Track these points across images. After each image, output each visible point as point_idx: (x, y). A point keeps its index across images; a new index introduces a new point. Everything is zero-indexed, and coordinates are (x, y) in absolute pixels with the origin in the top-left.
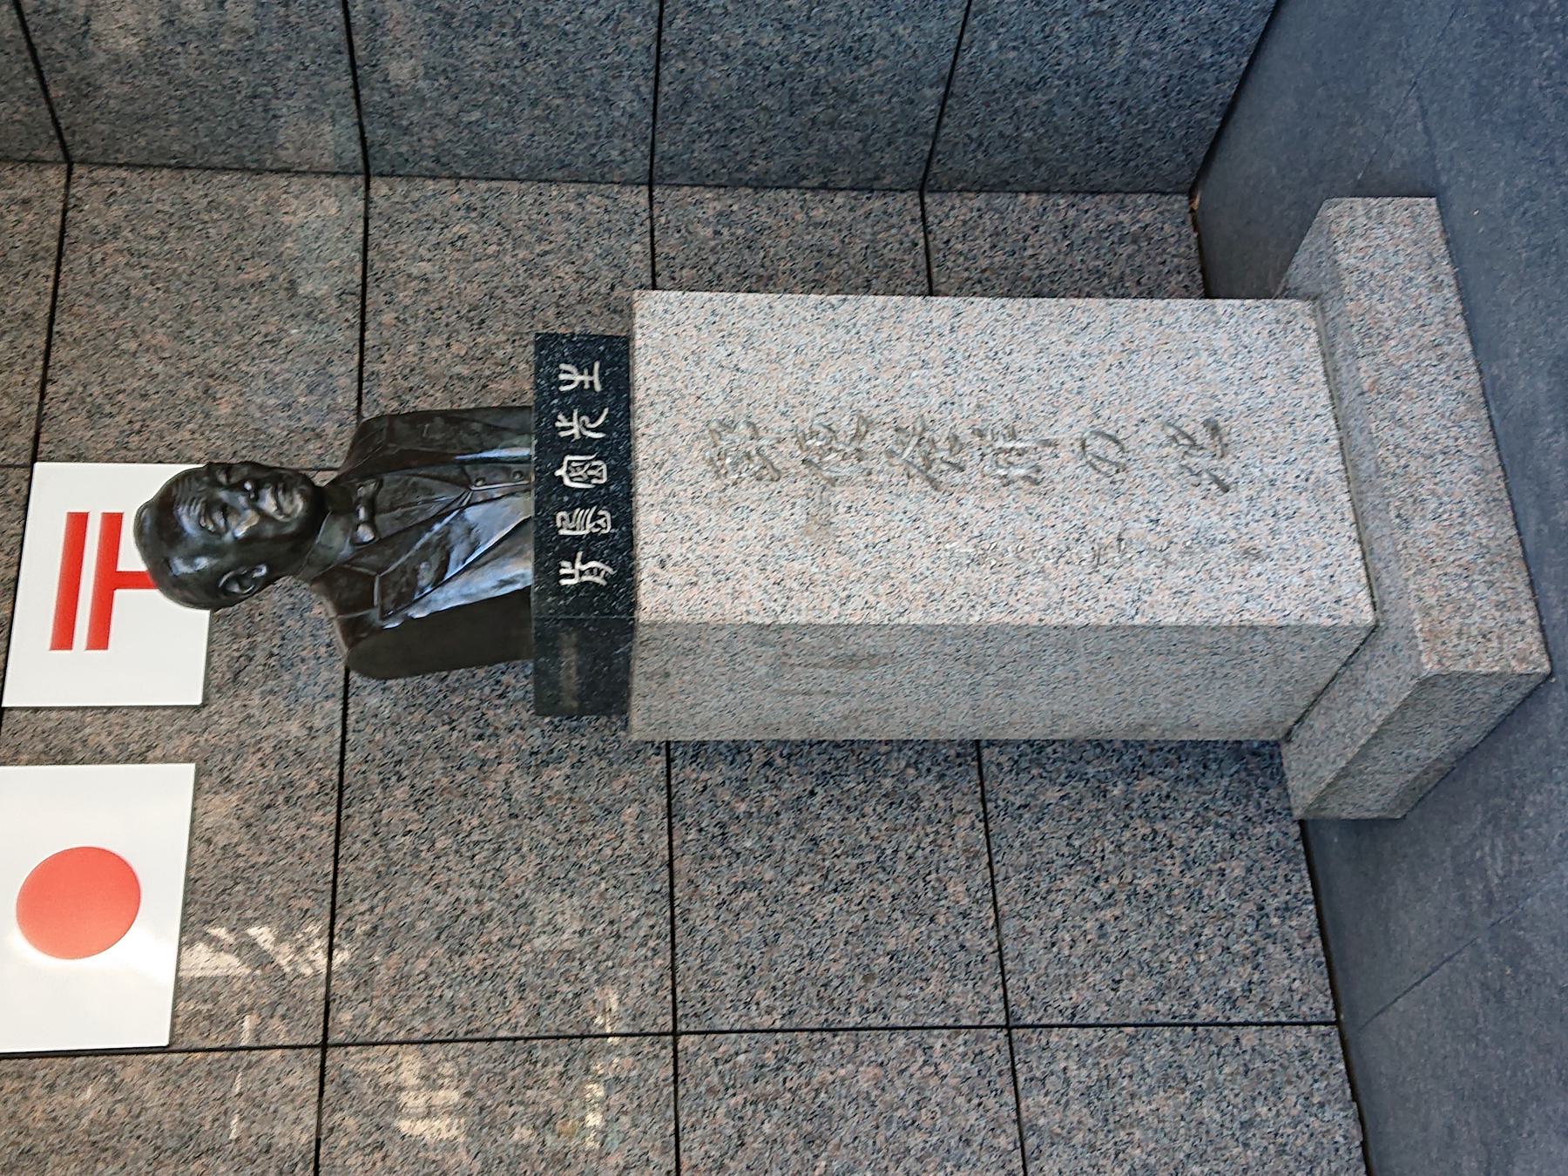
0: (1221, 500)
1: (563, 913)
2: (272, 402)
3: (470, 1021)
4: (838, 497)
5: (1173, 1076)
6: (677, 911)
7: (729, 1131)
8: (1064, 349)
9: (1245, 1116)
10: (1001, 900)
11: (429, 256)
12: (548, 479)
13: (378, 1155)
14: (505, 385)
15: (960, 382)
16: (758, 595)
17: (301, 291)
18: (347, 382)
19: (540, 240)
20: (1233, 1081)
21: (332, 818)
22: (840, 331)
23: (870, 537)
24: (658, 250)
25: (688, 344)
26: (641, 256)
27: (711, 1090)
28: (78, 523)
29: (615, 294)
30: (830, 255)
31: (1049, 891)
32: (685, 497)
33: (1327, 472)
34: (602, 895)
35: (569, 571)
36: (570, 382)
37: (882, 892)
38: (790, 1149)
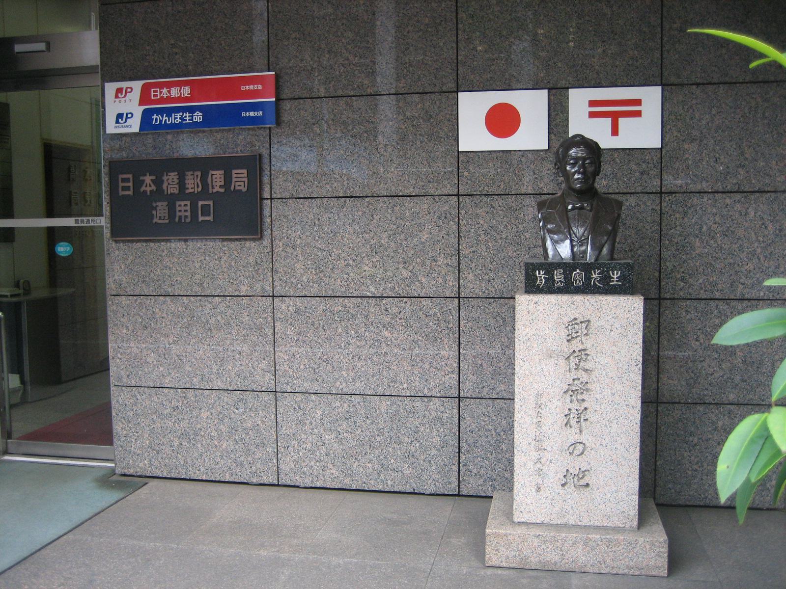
0: (559, 484)
1: (497, 264)
2: (690, 162)
3: (465, 237)
4: (561, 361)
5: (444, 444)
6: (497, 300)
7: (430, 313)
8: (619, 442)
9: (432, 462)
10: (498, 401)
11: (757, 215)
12: (575, 266)
13: (427, 212)
14: (698, 244)
15: (606, 406)
16: (525, 333)
17: (739, 169)
18: (699, 187)
19: (766, 257)
20: (442, 461)
21: (530, 192)
22: (627, 367)
23: (546, 370)
24: (761, 302)
25: (621, 315)
26: (758, 295)
27: (442, 308)
28: (638, 102)
29: (740, 285)
30: (758, 367)
31: (501, 416)
32: (561, 311)
33: (568, 519)
34: (502, 276)
35: (541, 273)
36: (613, 274)
37: (501, 364)
38: (425, 330)
